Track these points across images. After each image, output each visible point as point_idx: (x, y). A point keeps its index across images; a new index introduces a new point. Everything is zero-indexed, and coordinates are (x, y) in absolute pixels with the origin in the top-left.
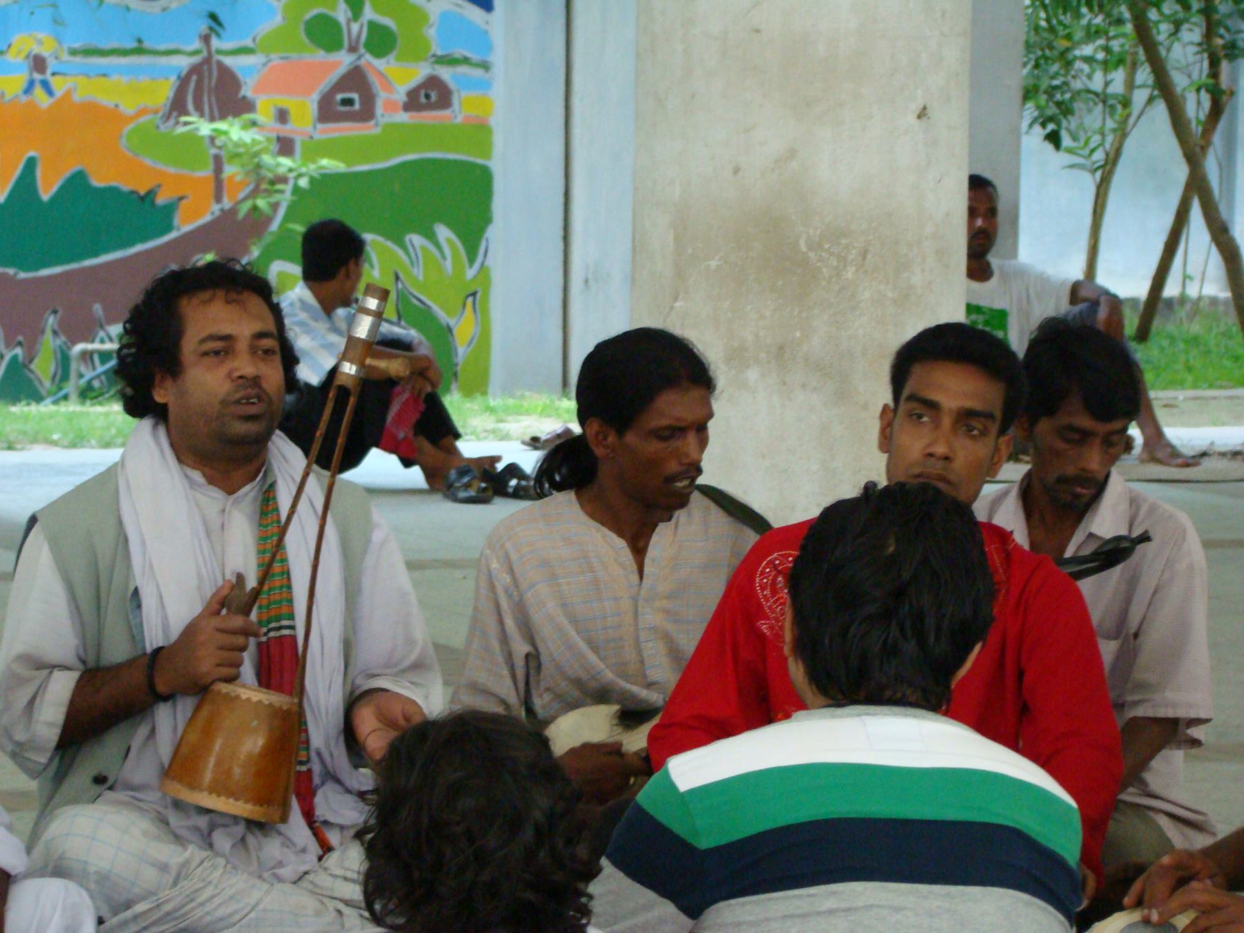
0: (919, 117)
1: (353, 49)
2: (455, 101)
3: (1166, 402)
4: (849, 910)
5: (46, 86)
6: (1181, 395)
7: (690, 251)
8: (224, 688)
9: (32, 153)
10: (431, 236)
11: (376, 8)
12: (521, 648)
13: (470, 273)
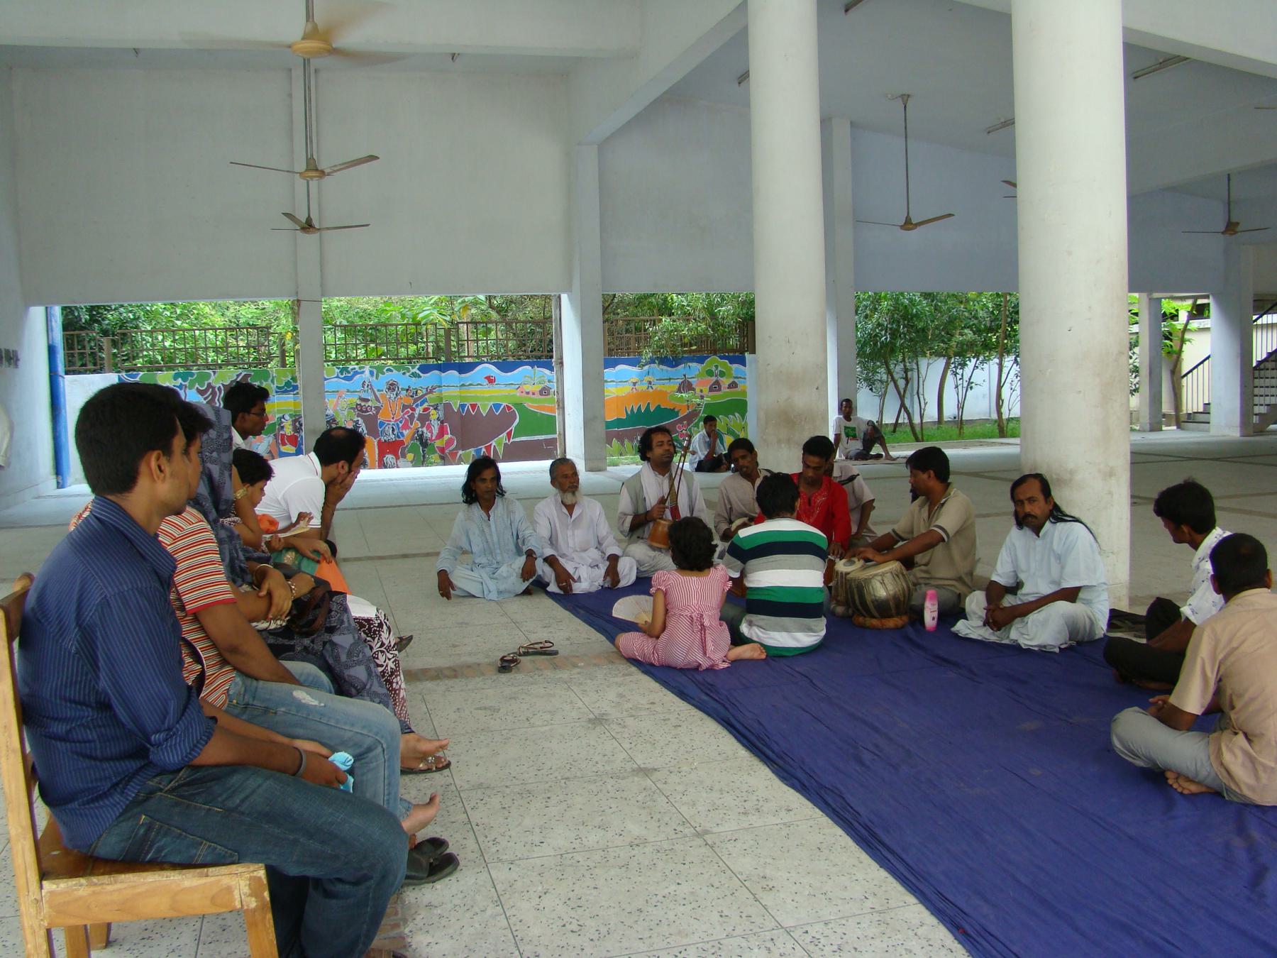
11: (721, 367)
12: (728, 506)
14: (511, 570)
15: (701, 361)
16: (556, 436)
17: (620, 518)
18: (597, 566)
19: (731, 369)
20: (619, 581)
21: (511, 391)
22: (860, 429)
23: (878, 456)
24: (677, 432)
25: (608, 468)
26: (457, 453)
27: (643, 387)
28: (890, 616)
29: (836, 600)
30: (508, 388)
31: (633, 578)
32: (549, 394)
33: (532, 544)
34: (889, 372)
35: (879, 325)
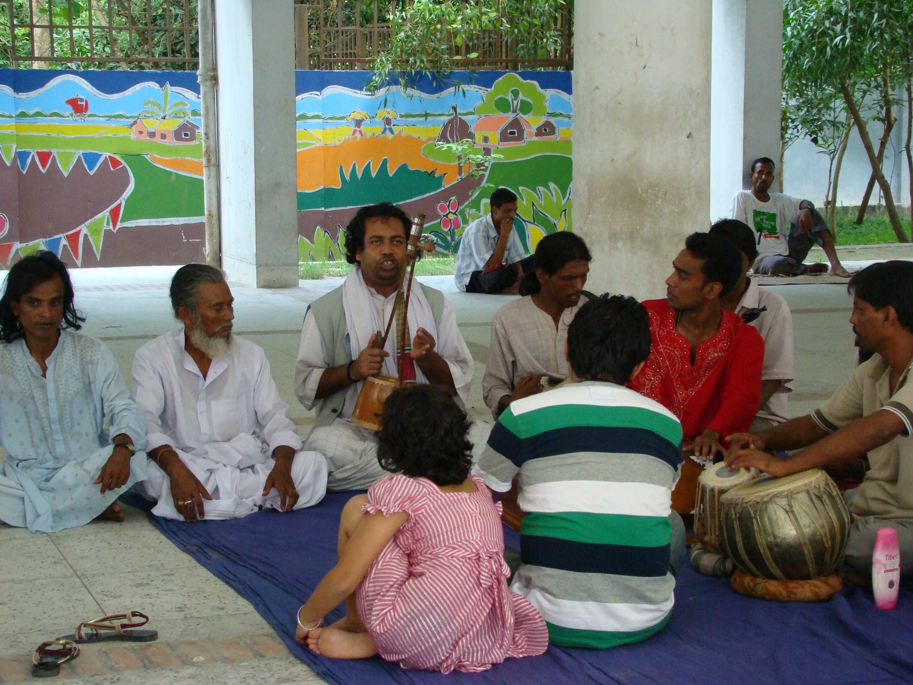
0: (688, 137)
1: (514, 111)
2: (557, 131)
3: (850, 250)
4: (578, 463)
5: (391, 130)
6: (857, 247)
7: (594, 194)
8: (370, 379)
9: (385, 158)
10: (547, 187)
12: (510, 359)
13: (564, 202)
14: (82, 473)
15: (486, 81)
16: (203, 219)
17: (299, 372)
18: (252, 467)
19: (543, 96)
20: (296, 497)
21: (119, 129)
22: (784, 220)
23: (819, 269)
24: (438, 216)
25: (302, 283)
26: (10, 247)
27: (373, 129)
28: (807, 577)
29: (702, 541)
30: (114, 124)
31: (320, 492)
32: (193, 138)
33: (127, 424)
34: (852, 109)
35: (831, 12)
